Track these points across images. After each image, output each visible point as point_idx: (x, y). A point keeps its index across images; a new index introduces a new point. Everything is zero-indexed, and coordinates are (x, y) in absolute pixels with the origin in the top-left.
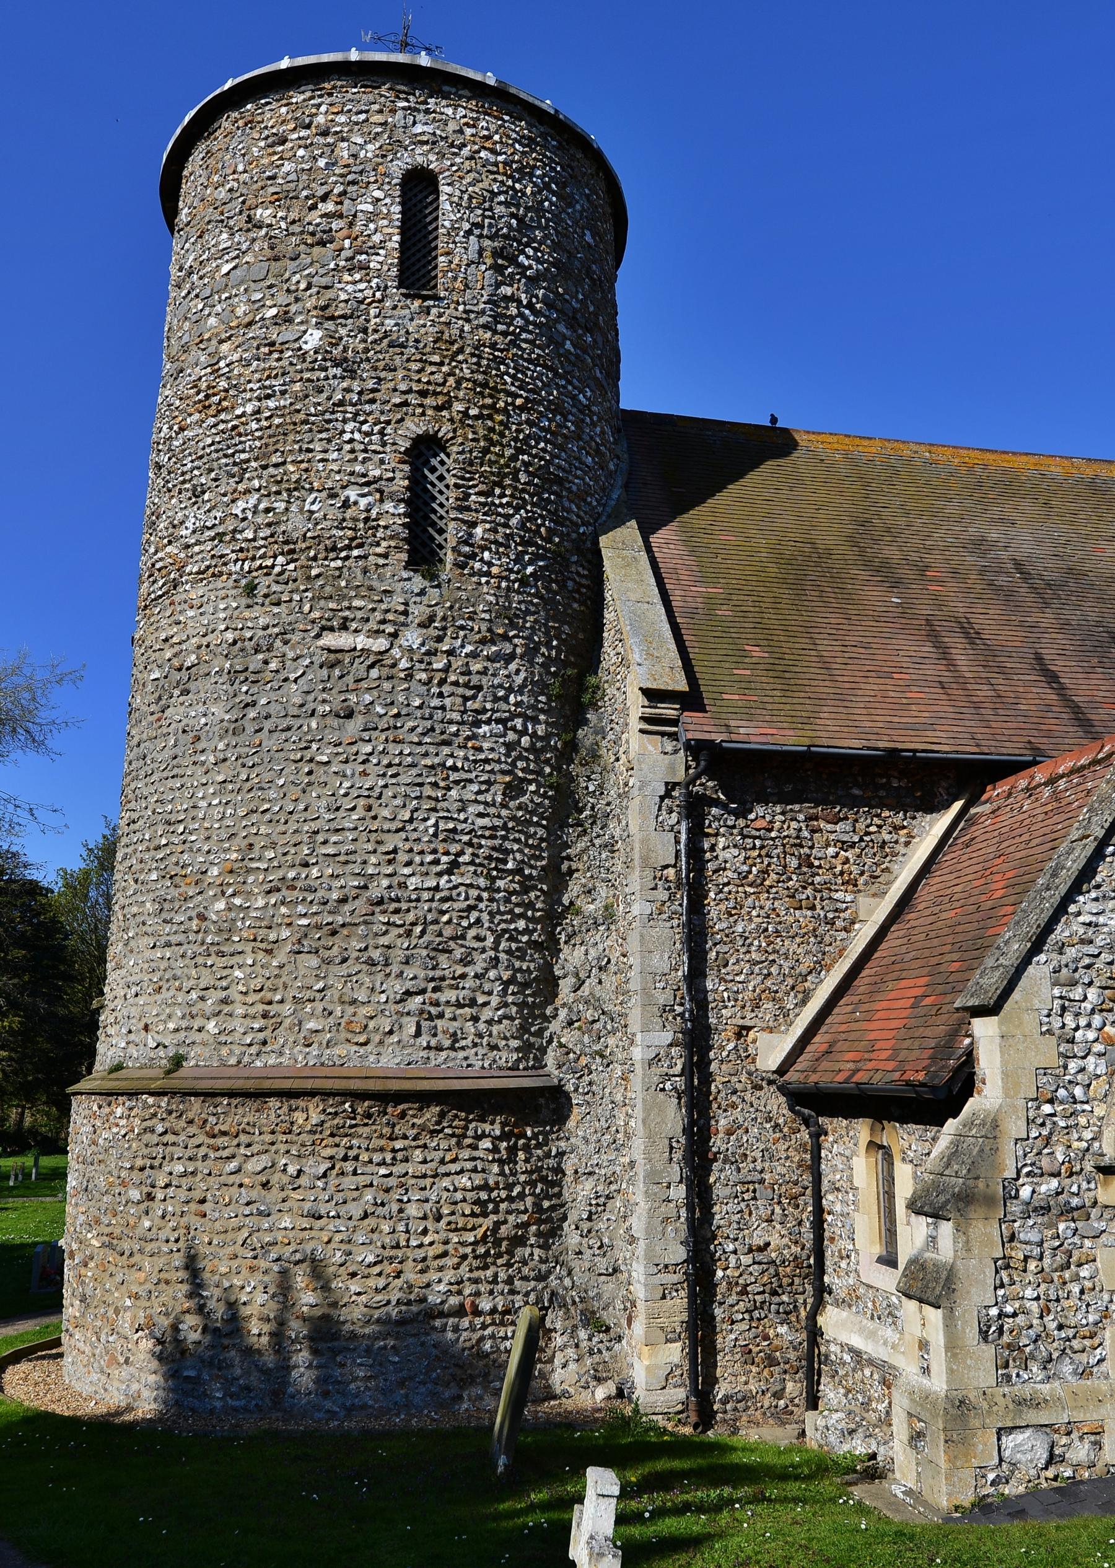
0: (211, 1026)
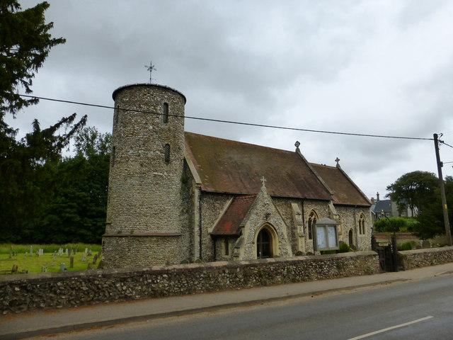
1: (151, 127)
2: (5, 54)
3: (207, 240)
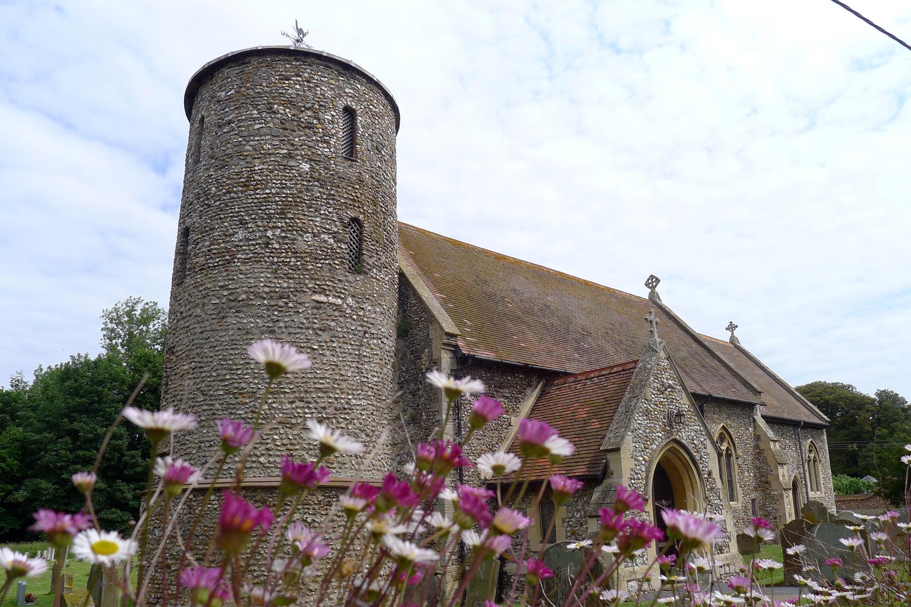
0: (262, 459)
1: (306, 167)
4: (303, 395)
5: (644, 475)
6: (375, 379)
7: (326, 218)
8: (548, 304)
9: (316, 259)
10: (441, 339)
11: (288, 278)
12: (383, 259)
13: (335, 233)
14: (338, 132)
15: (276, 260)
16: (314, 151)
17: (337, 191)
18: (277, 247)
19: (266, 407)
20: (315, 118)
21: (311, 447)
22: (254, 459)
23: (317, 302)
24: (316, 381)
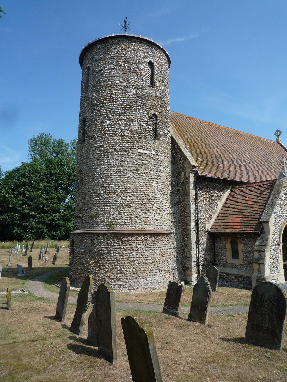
1: (134, 91)
2: (128, 380)
3: (204, 239)
4: (135, 194)
5: (279, 233)
6: (163, 186)
7: (143, 114)
8: (232, 147)
9: (139, 133)
10: (190, 168)
11: (128, 142)
12: (165, 132)
13: (146, 121)
14: (146, 74)
15: (123, 134)
16: (137, 83)
17: (147, 102)
18: (123, 128)
19: (120, 199)
20: (137, 68)
21: (139, 216)
22: (116, 221)
23: (140, 153)
24: (140, 187)
